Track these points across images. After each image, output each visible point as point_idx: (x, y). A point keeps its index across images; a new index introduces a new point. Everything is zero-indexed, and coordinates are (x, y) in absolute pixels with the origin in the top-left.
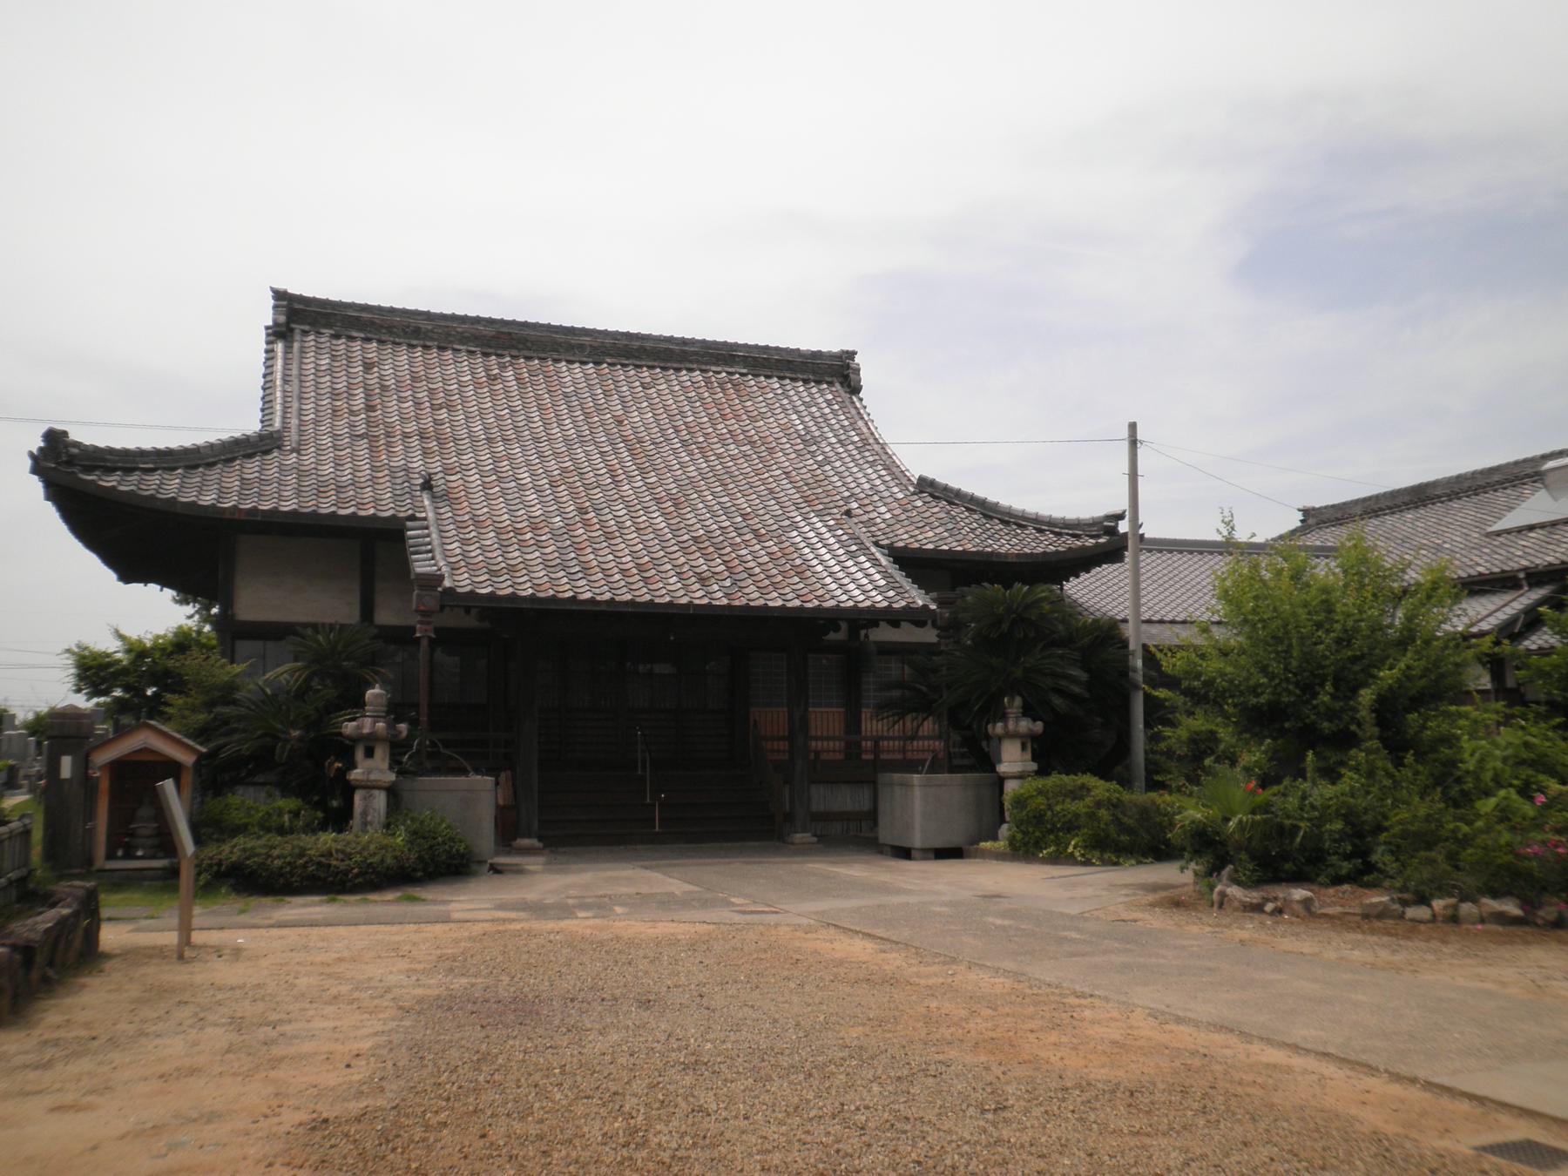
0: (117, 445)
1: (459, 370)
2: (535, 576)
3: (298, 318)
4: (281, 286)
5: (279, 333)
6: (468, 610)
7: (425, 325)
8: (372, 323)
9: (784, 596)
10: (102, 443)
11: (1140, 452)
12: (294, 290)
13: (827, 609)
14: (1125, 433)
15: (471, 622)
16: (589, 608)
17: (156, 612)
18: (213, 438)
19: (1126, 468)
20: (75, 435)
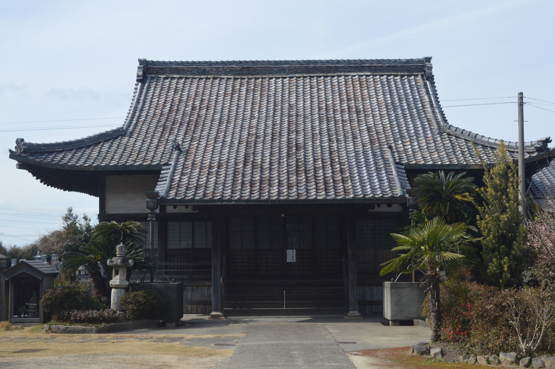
0: (47, 142)
1: (219, 87)
2: (221, 188)
3: (149, 71)
4: (142, 57)
5: (142, 80)
6: (187, 207)
7: (207, 67)
8: (183, 70)
9: (337, 193)
10: (40, 142)
11: (524, 106)
12: (149, 59)
13: (348, 199)
14: (516, 100)
15: (189, 210)
16: (424, 168)
17: (86, 207)
18: (109, 129)
19: (516, 116)
20: (27, 141)
